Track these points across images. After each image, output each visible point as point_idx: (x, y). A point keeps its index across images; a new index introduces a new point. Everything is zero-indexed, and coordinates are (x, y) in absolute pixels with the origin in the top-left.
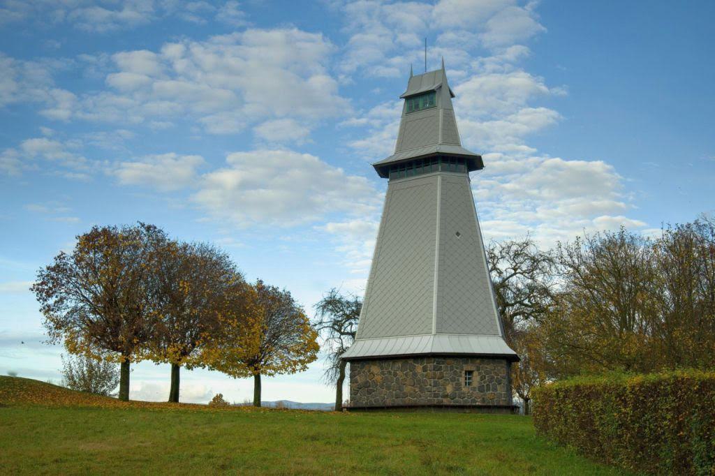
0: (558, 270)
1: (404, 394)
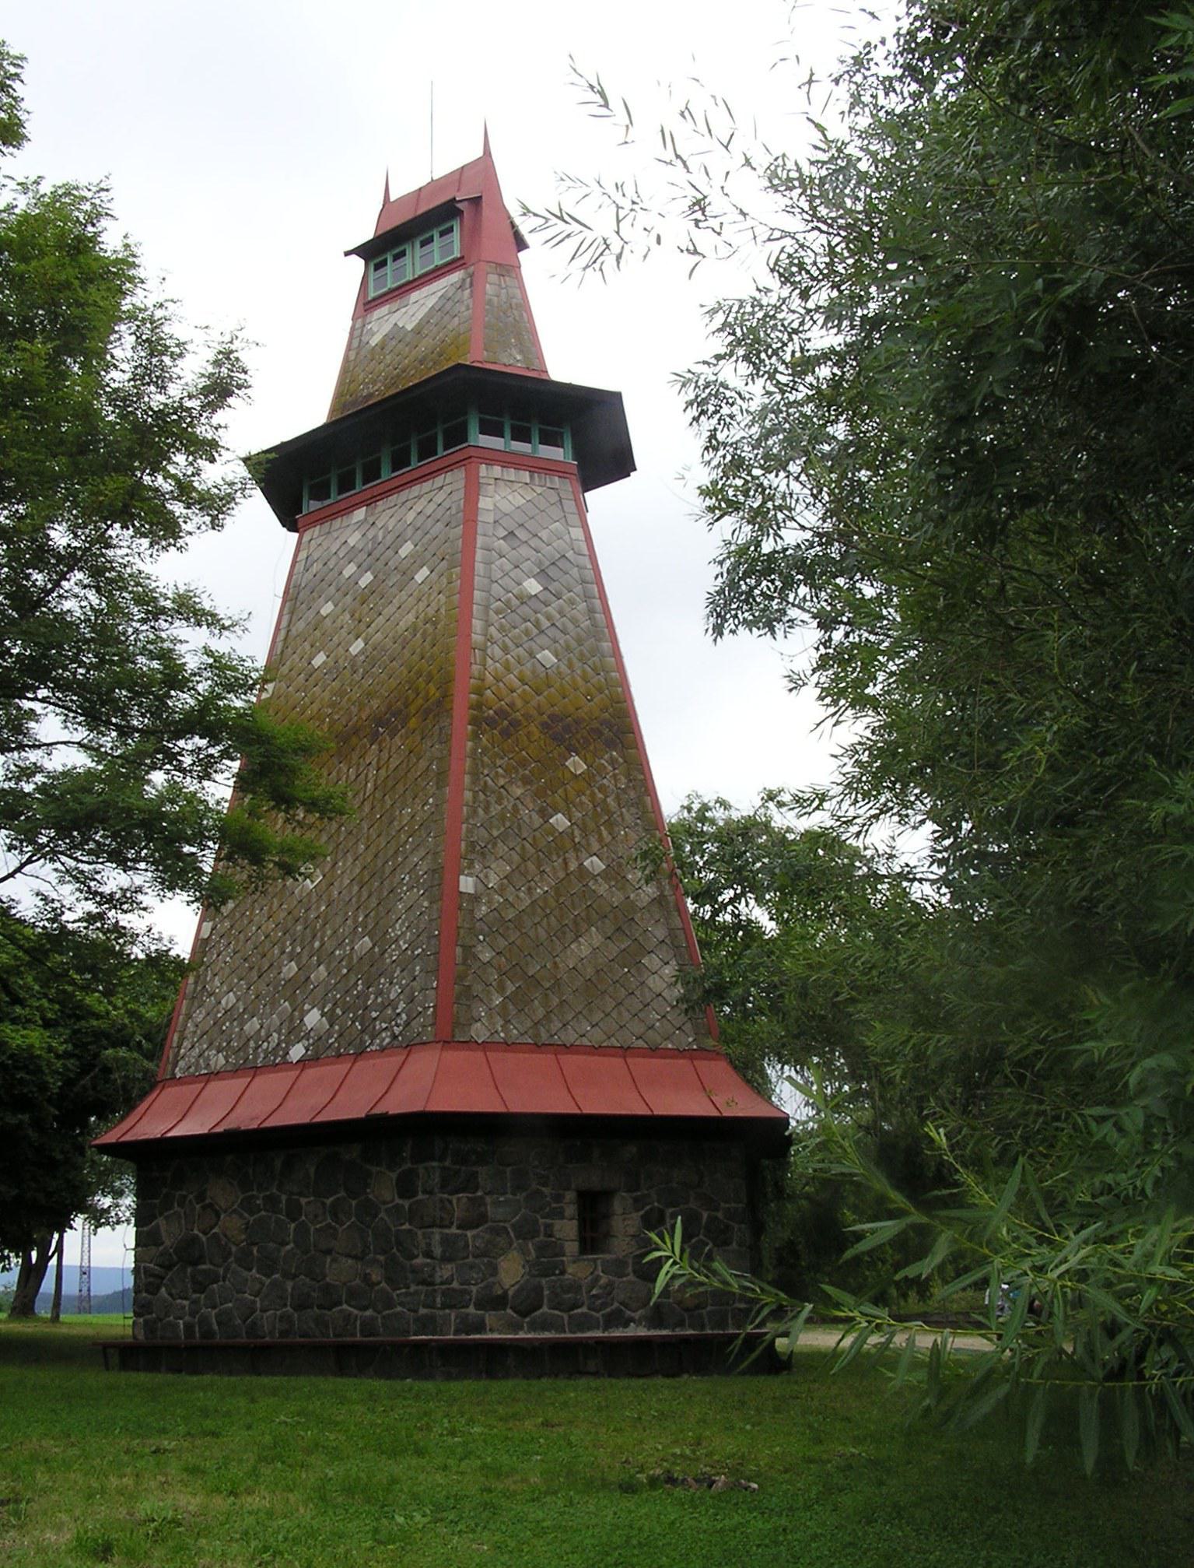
0: (565, 859)
1: (327, 1289)
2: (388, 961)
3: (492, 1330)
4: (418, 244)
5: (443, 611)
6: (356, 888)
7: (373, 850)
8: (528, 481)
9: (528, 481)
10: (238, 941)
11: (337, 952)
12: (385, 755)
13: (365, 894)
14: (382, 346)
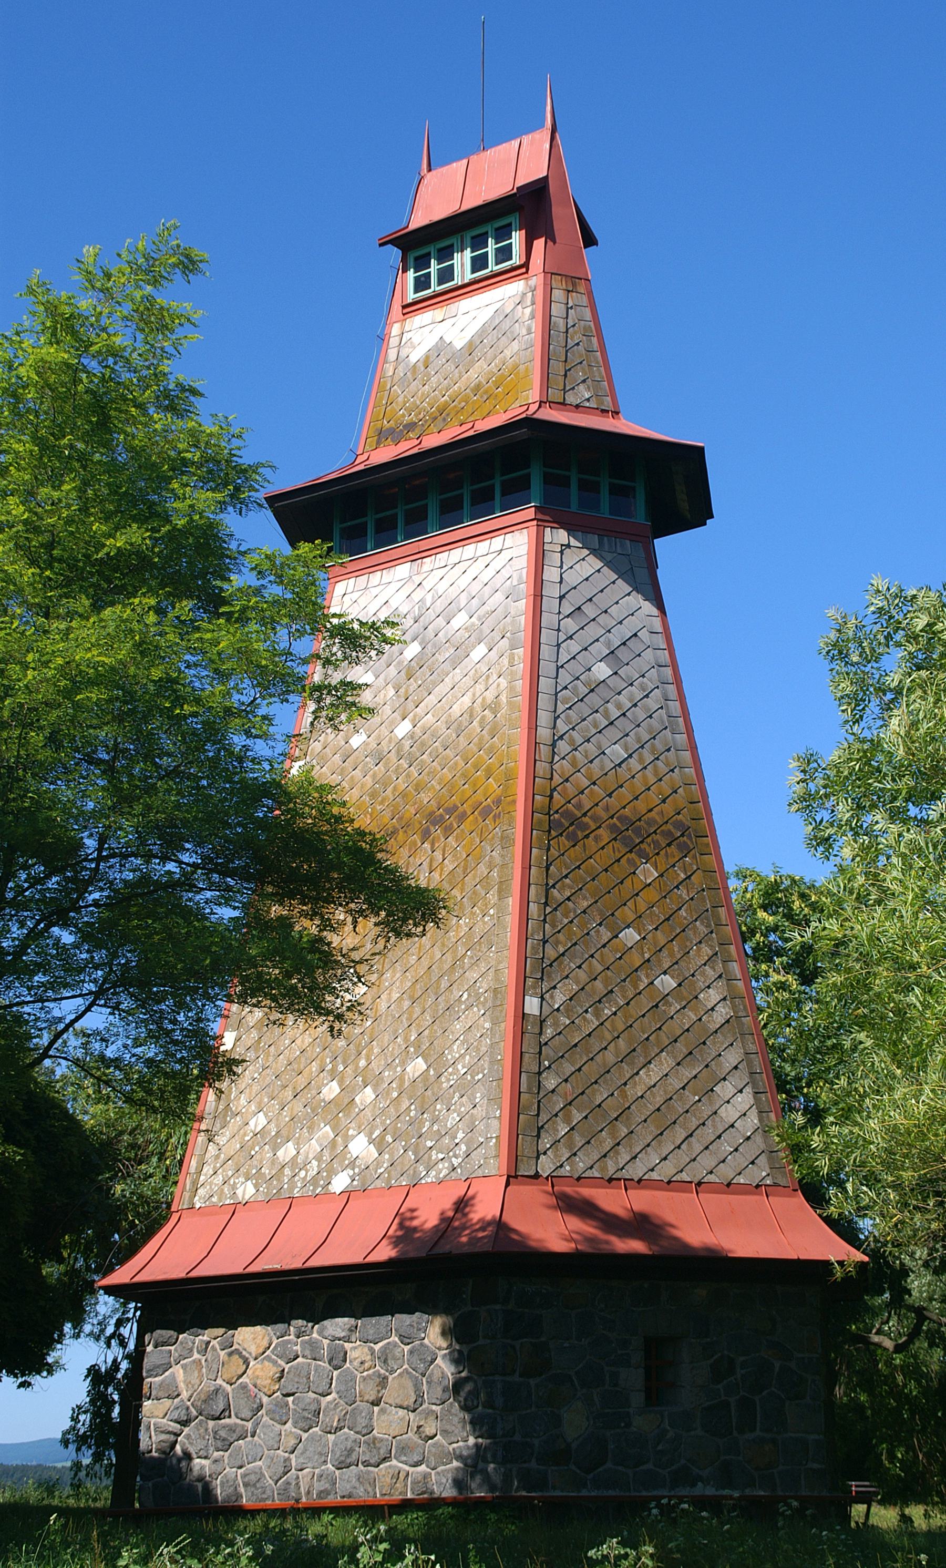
2: (445, 1085)
3: (554, 1488)
4: (468, 240)
5: (503, 698)
6: (407, 1003)
7: (425, 963)
8: (597, 547)
9: (597, 547)
10: (268, 1055)
11: (387, 1073)
12: (438, 855)
13: (417, 1010)
14: (427, 362)
